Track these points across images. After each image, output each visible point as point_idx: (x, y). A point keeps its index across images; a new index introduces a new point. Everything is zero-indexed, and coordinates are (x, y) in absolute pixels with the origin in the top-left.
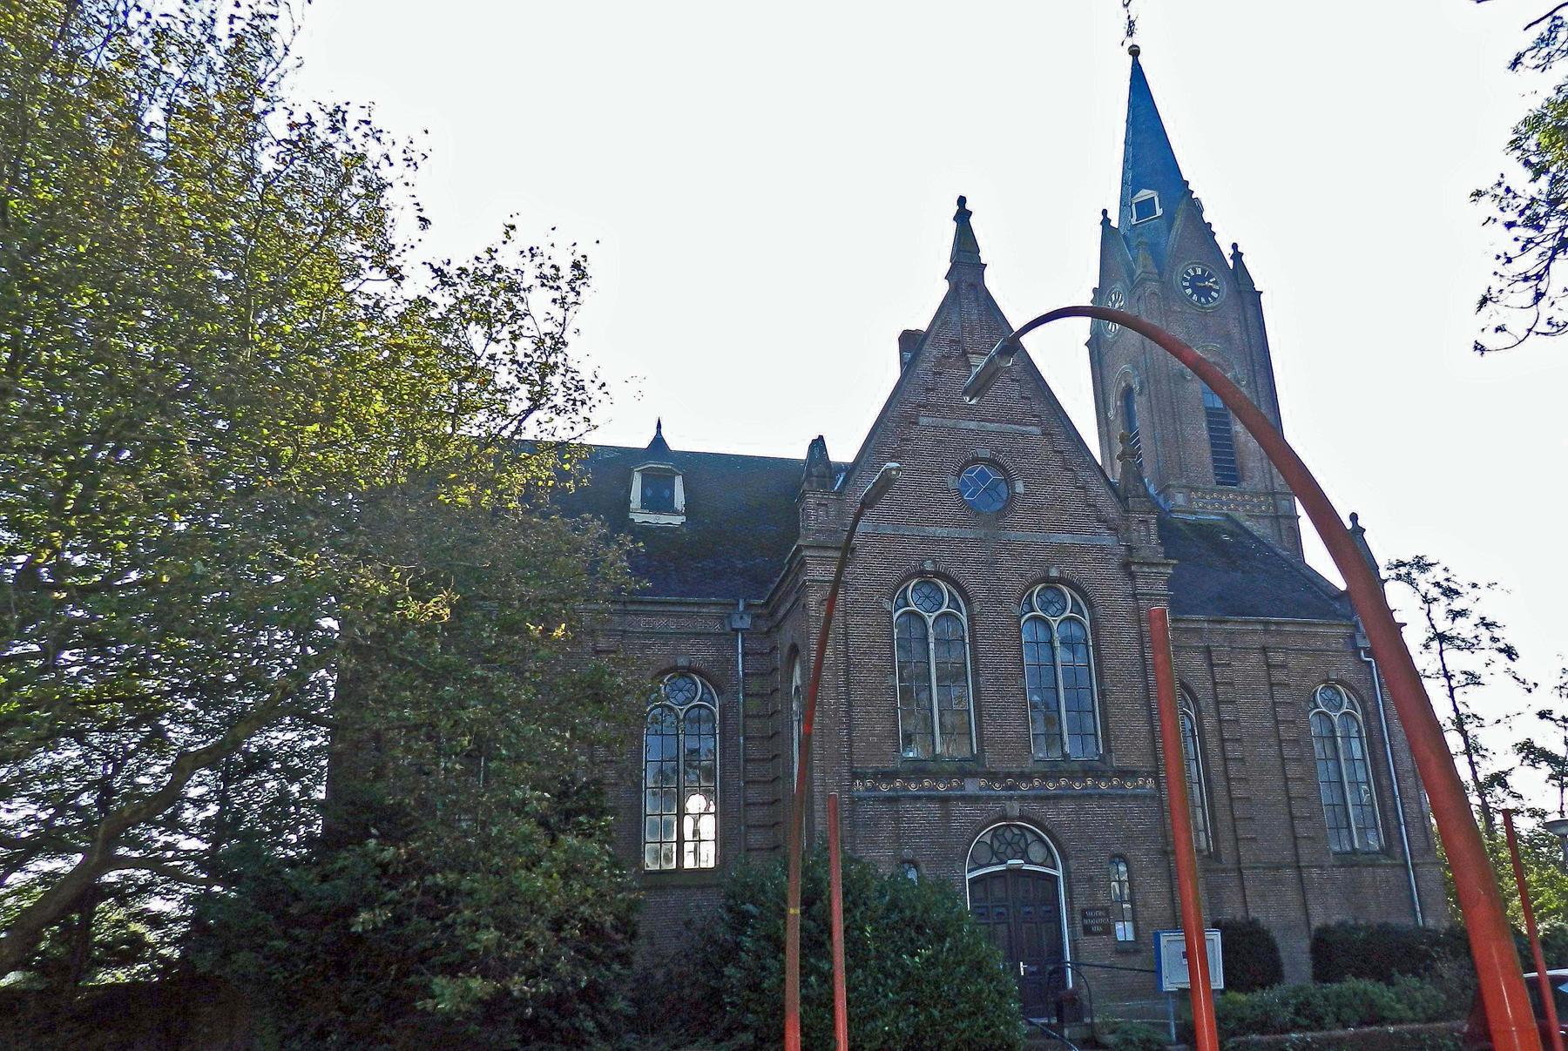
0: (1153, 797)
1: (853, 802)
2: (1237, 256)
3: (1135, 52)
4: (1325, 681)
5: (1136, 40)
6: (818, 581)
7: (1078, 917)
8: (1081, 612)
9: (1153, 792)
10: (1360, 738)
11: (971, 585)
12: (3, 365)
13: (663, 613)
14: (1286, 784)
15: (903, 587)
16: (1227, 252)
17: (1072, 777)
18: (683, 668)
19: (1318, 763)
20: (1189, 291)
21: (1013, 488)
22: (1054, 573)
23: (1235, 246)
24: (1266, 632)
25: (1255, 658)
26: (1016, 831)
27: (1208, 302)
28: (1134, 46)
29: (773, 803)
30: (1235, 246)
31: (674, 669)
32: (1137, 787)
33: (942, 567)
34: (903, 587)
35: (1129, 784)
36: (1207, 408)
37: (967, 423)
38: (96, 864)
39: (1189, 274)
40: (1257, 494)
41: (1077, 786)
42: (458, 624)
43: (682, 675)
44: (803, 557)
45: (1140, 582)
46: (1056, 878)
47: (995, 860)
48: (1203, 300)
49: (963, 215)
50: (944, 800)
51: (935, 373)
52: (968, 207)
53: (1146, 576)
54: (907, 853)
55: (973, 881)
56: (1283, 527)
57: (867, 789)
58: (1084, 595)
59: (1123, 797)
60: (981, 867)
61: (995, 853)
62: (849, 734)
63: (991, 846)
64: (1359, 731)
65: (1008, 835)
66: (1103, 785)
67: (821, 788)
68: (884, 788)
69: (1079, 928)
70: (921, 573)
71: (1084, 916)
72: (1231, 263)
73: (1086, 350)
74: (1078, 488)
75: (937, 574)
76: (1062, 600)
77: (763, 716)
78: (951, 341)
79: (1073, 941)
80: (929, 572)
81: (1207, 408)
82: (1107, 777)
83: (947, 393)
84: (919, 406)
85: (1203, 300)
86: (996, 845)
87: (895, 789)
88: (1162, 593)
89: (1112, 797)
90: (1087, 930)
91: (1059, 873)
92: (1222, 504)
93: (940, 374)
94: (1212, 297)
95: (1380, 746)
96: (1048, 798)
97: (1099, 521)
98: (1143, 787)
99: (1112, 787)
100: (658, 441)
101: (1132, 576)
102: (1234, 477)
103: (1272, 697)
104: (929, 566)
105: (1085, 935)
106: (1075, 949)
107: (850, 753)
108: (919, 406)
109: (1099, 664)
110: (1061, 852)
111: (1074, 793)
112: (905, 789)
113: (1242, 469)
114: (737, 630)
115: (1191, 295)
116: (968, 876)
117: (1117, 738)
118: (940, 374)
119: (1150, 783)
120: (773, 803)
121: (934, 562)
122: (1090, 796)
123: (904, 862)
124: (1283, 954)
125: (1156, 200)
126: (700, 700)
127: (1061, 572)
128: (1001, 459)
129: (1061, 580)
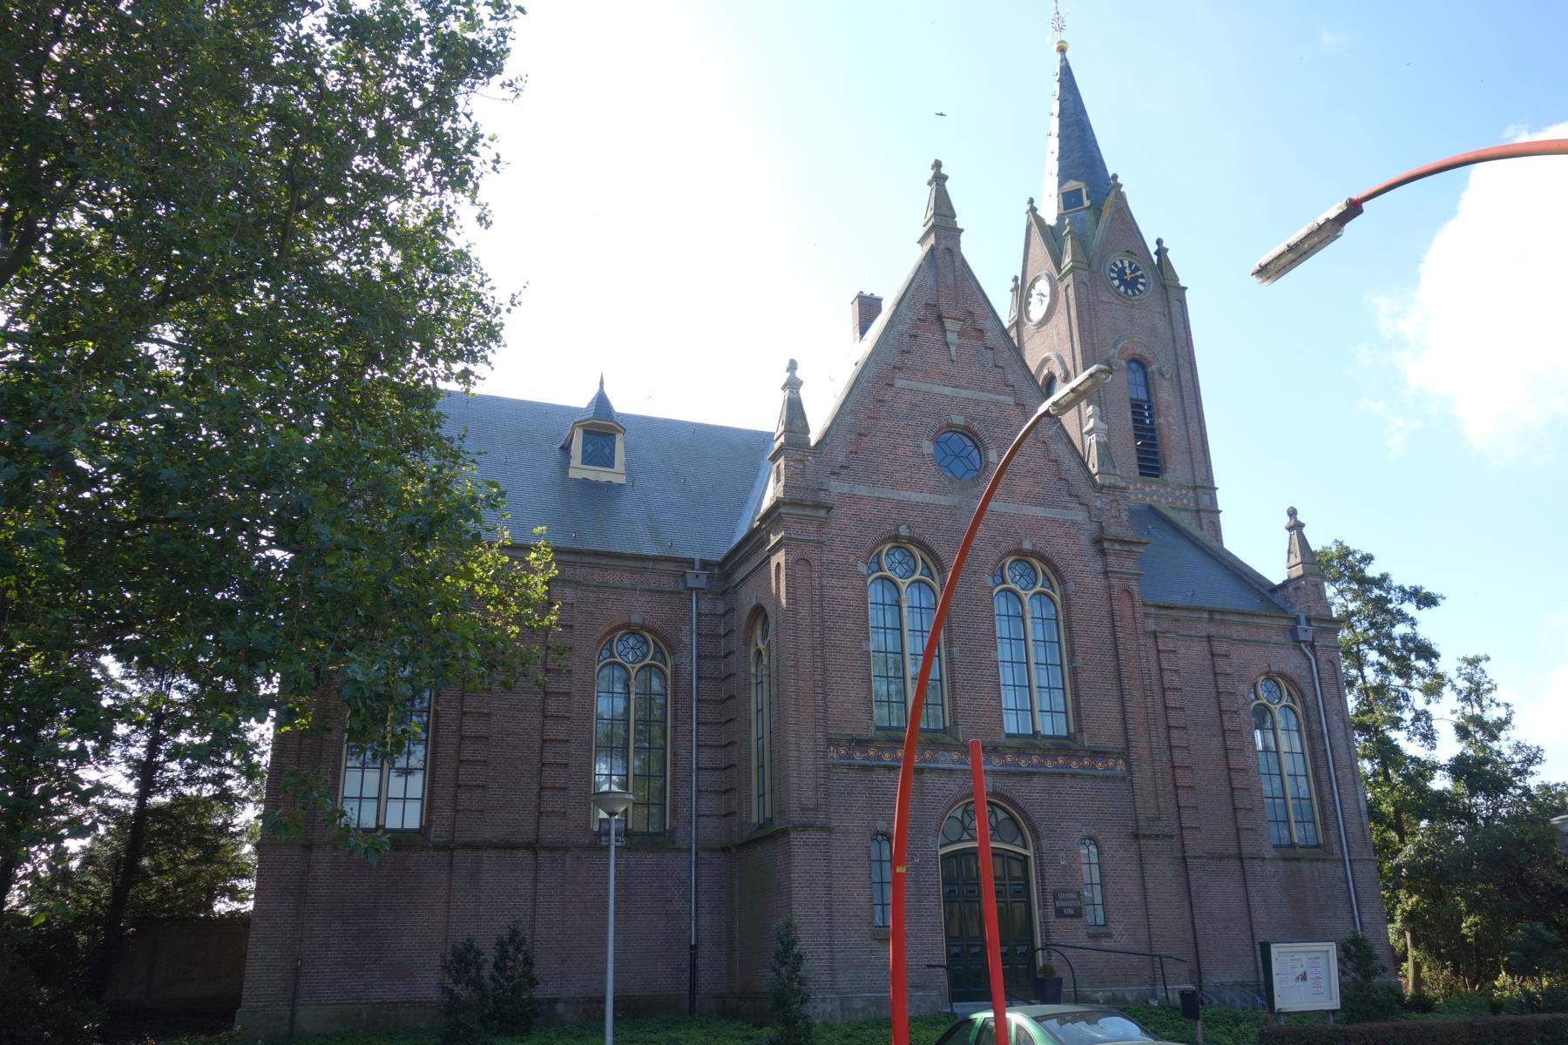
0: (1123, 779)
1: (828, 770)
2: (1161, 252)
4: (1267, 673)
5: (1064, 36)
6: (797, 540)
7: (1050, 897)
8: (1051, 586)
10: (1299, 731)
12: (2, 214)
13: (617, 568)
14: (1229, 774)
15: (876, 551)
16: (1153, 248)
17: (1044, 754)
18: (636, 625)
19: (1260, 755)
20: (1116, 283)
21: (986, 457)
22: (1027, 545)
23: (1159, 242)
24: (1211, 620)
25: (1200, 648)
27: (1134, 294)
28: (1062, 42)
29: (726, 768)
30: (1159, 242)
31: (627, 625)
32: (1108, 768)
34: (876, 551)
36: (1131, 399)
37: (941, 388)
38: (215, 825)
39: (1116, 266)
40: (1180, 487)
41: (1049, 763)
43: (633, 633)
44: (780, 514)
45: (1111, 559)
46: (1026, 857)
47: (966, 836)
48: (1130, 292)
49: (939, 179)
51: (911, 336)
53: (1117, 554)
55: (944, 856)
56: (1204, 521)
57: (841, 757)
58: (1055, 570)
59: (1094, 777)
60: (952, 843)
62: (824, 699)
63: (962, 822)
64: (1298, 724)
66: (1023, 762)
68: (858, 756)
69: (1051, 911)
70: (896, 538)
71: (1056, 898)
72: (1155, 258)
73: (1182, 283)
74: (1050, 460)
77: (716, 678)
78: (927, 304)
79: (1045, 923)
80: (904, 537)
81: (1131, 399)
82: (1078, 756)
83: (922, 357)
84: (895, 368)
85: (1130, 292)
87: (868, 758)
88: (1133, 572)
89: (1084, 776)
90: (1059, 913)
91: (1030, 853)
92: (1145, 494)
93: (916, 336)
94: (1139, 290)
95: (1320, 740)
96: (1022, 774)
97: (1070, 495)
98: (1114, 768)
99: (1083, 767)
100: (601, 402)
101: (1103, 553)
102: (1157, 469)
103: (1216, 686)
104: (903, 531)
106: (1046, 932)
107: (825, 719)
108: (895, 368)
110: (1034, 830)
111: (1047, 770)
112: (880, 758)
113: (1165, 463)
114: (691, 589)
115: (1118, 287)
118: (916, 336)
119: (1121, 766)
120: (726, 768)
121: (909, 527)
122: (1063, 775)
123: (878, 834)
125: (1084, 191)
126: (652, 659)
127: (1034, 545)
128: (976, 427)
129: (1034, 554)
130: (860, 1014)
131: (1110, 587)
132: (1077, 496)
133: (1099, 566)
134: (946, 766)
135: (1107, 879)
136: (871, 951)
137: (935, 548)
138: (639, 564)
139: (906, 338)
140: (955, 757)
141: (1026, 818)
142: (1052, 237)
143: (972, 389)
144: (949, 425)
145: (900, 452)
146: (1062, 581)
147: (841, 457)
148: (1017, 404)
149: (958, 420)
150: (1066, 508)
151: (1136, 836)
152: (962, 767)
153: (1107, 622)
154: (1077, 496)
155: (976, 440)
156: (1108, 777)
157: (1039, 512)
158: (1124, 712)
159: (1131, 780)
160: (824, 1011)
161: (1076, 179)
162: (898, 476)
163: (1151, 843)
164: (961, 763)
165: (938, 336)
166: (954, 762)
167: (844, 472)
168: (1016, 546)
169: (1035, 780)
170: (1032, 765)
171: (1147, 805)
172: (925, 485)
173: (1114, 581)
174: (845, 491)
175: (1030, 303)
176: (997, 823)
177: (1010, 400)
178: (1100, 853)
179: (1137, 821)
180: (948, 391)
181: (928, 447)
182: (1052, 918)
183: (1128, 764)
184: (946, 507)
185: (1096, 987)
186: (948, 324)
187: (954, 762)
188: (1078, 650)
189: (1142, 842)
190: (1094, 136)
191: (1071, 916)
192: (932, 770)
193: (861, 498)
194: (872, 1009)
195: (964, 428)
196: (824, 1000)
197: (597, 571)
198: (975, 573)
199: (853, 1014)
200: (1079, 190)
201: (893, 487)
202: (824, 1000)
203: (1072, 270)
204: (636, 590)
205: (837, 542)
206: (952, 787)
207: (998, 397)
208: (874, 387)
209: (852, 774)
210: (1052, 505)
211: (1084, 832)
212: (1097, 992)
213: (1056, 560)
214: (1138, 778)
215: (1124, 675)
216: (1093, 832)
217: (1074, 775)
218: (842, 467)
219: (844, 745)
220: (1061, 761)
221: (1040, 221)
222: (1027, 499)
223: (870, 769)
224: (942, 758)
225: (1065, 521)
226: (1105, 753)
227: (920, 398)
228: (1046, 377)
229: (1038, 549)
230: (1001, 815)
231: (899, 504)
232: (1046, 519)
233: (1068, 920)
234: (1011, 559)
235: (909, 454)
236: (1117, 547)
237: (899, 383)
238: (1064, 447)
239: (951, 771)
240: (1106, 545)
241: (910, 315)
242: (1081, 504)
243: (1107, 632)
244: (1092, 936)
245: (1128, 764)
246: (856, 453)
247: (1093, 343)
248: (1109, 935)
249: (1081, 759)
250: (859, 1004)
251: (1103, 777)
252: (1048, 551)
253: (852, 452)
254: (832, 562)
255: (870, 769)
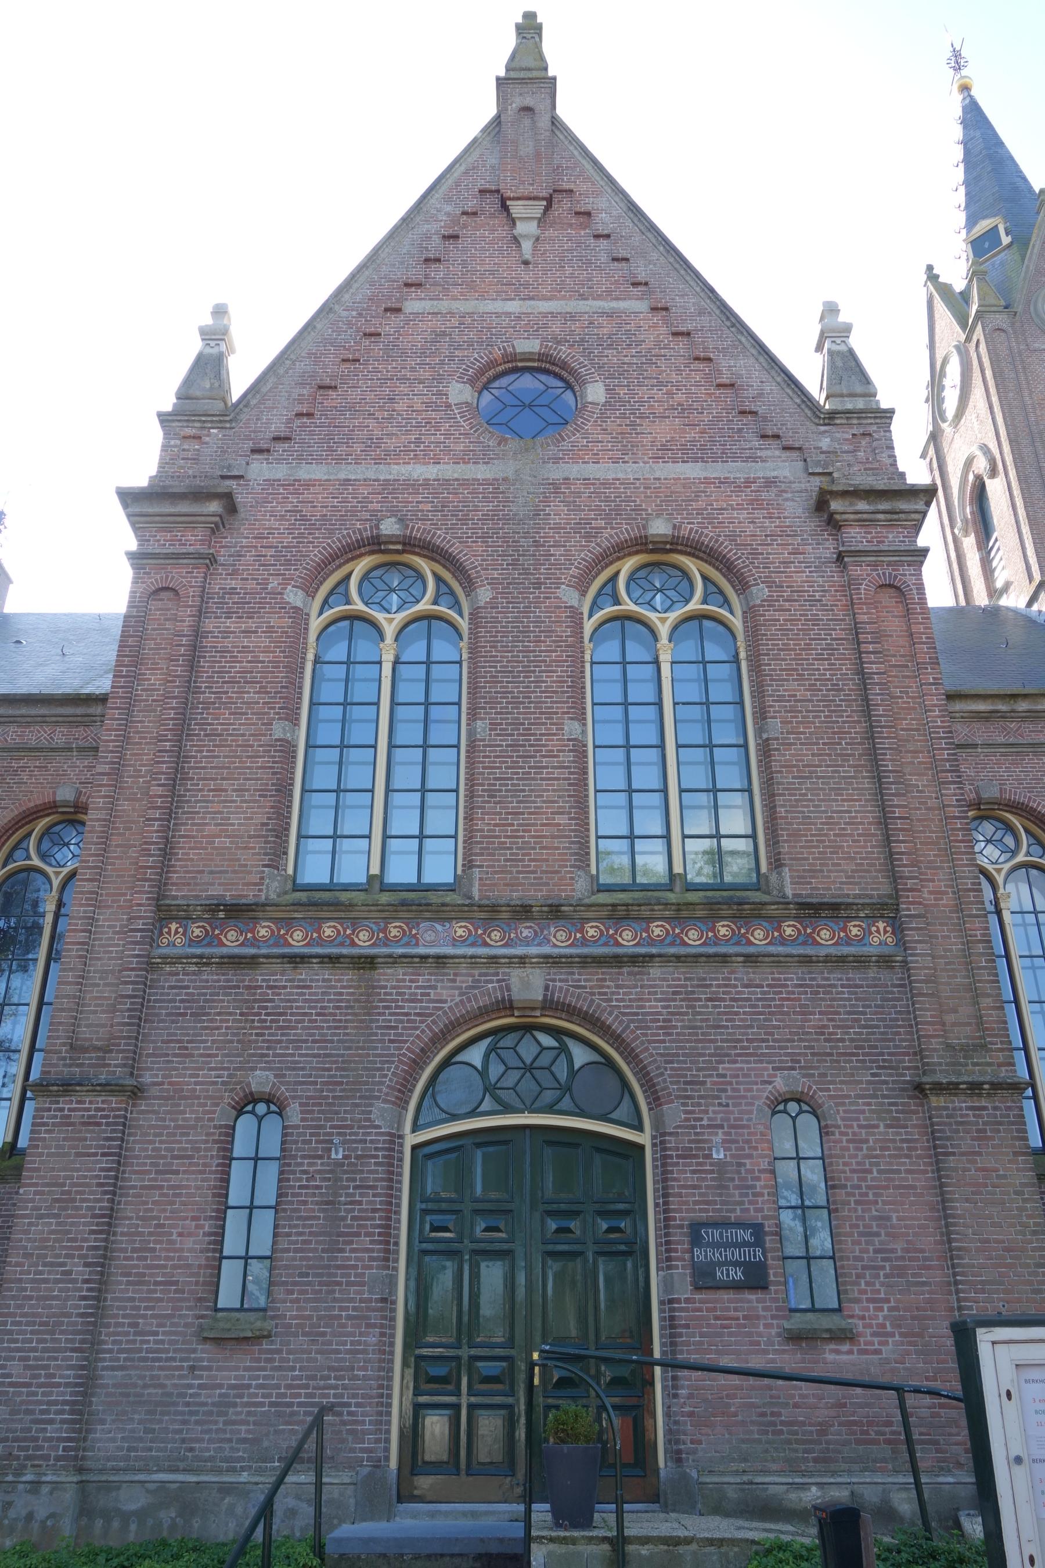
3: (965, 88)
7: (680, 1238)
8: (726, 603)
9: (886, 950)
11: (471, 555)
22: (659, 528)
26: (547, 1040)
32: (848, 941)
33: (419, 530)
35: (825, 934)
42: (549, 1363)
46: (641, 1148)
50: (367, 963)
51: (445, 237)
52: (551, 47)
54: (260, 1080)
57: (192, 943)
58: (727, 567)
59: (806, 960)
61: (490, 1089)
65: (527, 1050)
66: (758, 936)
67: (81, 936)
68: (232, 941)
69: (682, 1273)
71: (696, 1240)
75: (410, 545)
76: (685, 583)
80: (392, 540)
82: (768, 918)
86: (495, 1070)
89: (778, 961)
91: (644, 1138)
96: (617, 961)
101: (833, 524)
105: (698, 1288)
109: (759, 693)
110: (649, 1086)
116: (411, 1139)
117: (795, 835)
121: (401, 520)
124: (527, 350)
128: (564, 352)
130: (133, 1527)
131: (850, 586)
132: (777, 437)
133: (828, 549)
134: (432, 951)
135: (841, 1194)
136: (192, 1368)
137: (454, 550)
138: (80, 711)
139: (436, 240)
140: (460, 932)
141: (631, 1056)
142: (957, 302)
143: (564, 298)
144: (512, 357)
145: (401, 406)
146: (742, 586)
147: (276, 423)
148: (654, 309)
149: (528, 346)
150: (754, 459)
151: (919, 1089)
152: (471, 951)
153: (845, 650)
154: (777, 437)
155: (564, 373)
156: (842, 960)
157: (693, 471)
158: (884, 820)
159: (905, 962)
160: (30, 1517)
161: (984, 218)
162: (391, 443)
163: (961, 1103)
164: (473, 944)
165: (502, 232)
166: (454, 942)
167: (281, 447)
168: (635, 533)
169: (655, 971)
170: (652, 942)
171: (949, 1018)
172: (448, 451)
173: (856, 571)
174: (279, 475)
175: (943, 399)
176: (573, 1073)
177: (641, 306)
178: (824, 1132)
179: (920, 1053)
180: (514, 306)
181: (459, 392)
182: (684, 1291)
183: (898, 928)
184: (486, 482)
185: (803, 1474)
186: (517, 209)
187: (454, 942)
188: (774, 707)
189: (935, 1101)
190: (1016, 165)
191: (736, 1286)
192: (394, 960)
193: (308, 484)
194: (167, 1516)
195: (542, 357)
196: (35, 1486)
197: (12, 728)
198: (538, 585)
199: (116, 1524)
200: (996, 228)
201: (378, 460)
202: (35, 1486)
203: (979, 315)
204: (70, 749)
205: (249, 558)
206: (445, 994)
207: (614, 304)
208: (360, 315)
209: (210, 976)
210: (724, 457)
211: (780, 1084)
212: (804, 1487)
213: (727, 548)
214: (921, 958)
215: (884, 744)
216: (800, 1083)
217: (751, 959)
218: (277, 439)
219: (200, 919)
220: (723, 931)
221: (945, 291)
222: (664, 452)
223: (251, 962)
224: (429, 936)
225: (748, 482)
226: (835, 907)
227: (455, 322)
228: (974, 485)
229: (684, 532)
230: (580, 1055)
231: (388, 486)
232: (707, 481)
233: (726, 1296)
234: (627, 566)
235: (418, 406)
236: (862, 506)
237: (412, 306)
238: (752, 360)
239: (441, 960)
240: (835, 505)
241: (448, 208)
242: (786, 448)
243: (847, 668)
244: (796, 1338)
245: (898, 928)
246: (310, 415)
247: (1024, 407)
248: (843, 1336)
249: (776, 922)
250: (132, 1500)
251: (828, 959)
252: (708, 535)
253: (299, 415)
254: (233, 591)
255: (251, 962)
